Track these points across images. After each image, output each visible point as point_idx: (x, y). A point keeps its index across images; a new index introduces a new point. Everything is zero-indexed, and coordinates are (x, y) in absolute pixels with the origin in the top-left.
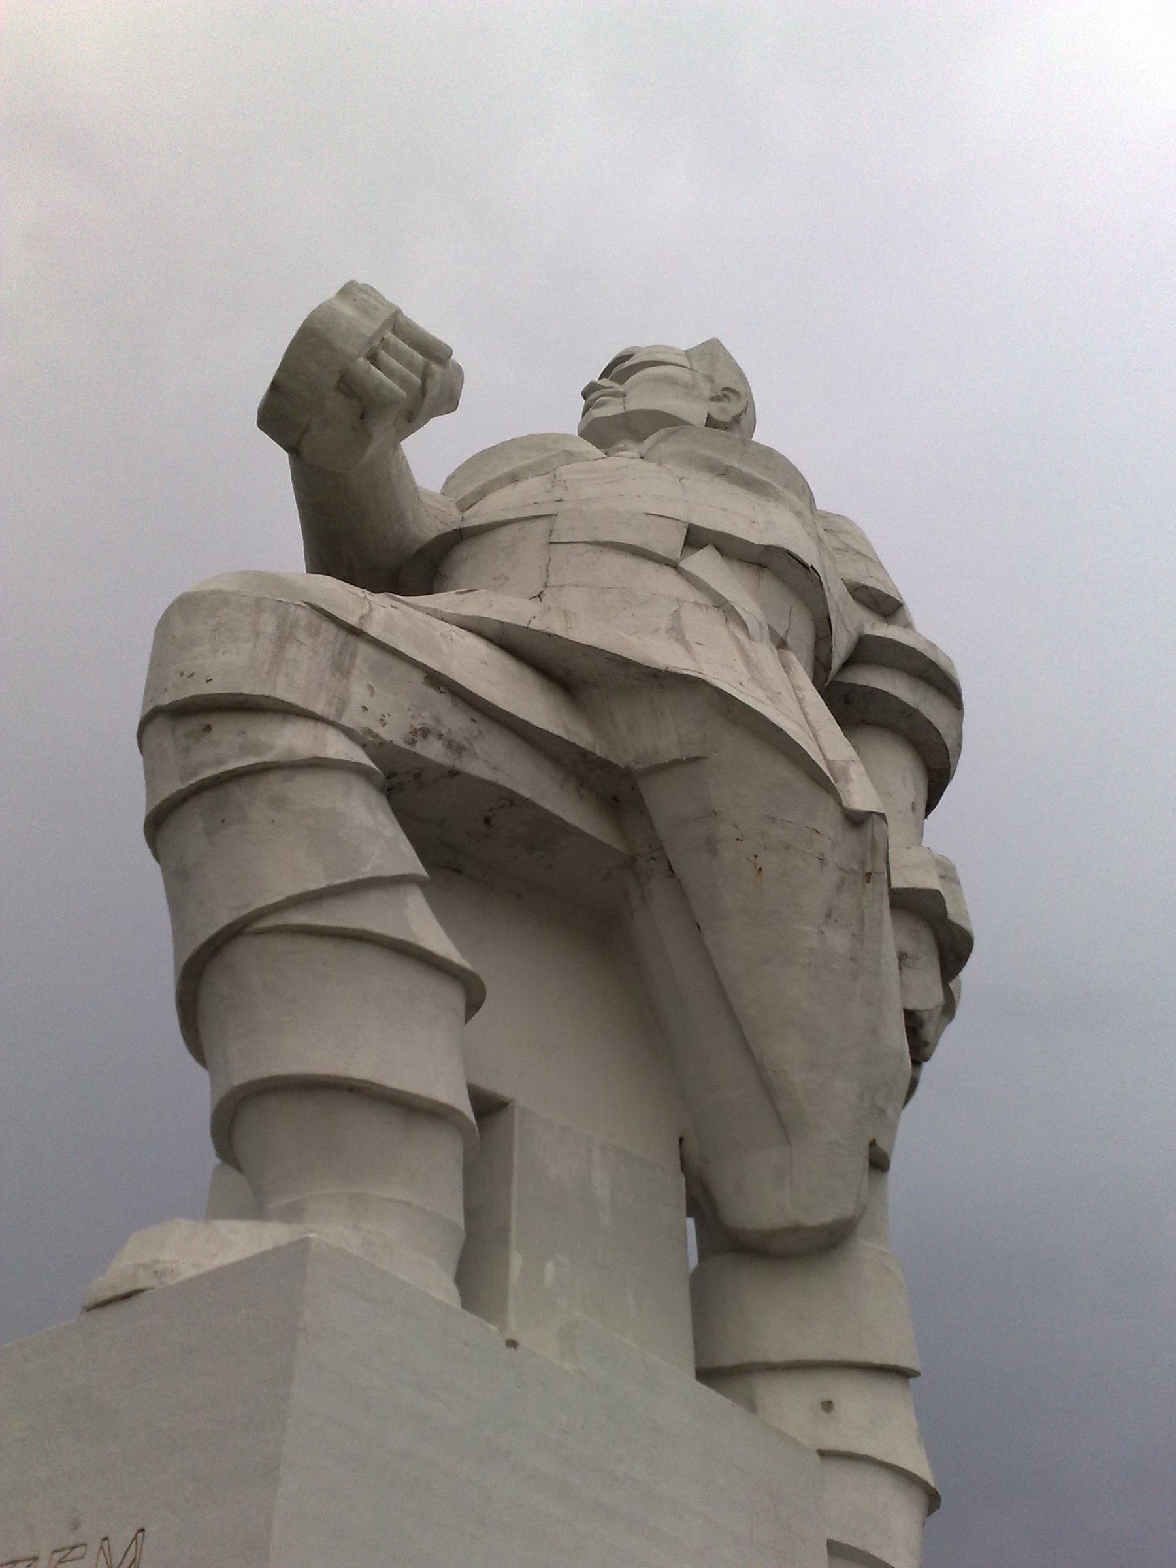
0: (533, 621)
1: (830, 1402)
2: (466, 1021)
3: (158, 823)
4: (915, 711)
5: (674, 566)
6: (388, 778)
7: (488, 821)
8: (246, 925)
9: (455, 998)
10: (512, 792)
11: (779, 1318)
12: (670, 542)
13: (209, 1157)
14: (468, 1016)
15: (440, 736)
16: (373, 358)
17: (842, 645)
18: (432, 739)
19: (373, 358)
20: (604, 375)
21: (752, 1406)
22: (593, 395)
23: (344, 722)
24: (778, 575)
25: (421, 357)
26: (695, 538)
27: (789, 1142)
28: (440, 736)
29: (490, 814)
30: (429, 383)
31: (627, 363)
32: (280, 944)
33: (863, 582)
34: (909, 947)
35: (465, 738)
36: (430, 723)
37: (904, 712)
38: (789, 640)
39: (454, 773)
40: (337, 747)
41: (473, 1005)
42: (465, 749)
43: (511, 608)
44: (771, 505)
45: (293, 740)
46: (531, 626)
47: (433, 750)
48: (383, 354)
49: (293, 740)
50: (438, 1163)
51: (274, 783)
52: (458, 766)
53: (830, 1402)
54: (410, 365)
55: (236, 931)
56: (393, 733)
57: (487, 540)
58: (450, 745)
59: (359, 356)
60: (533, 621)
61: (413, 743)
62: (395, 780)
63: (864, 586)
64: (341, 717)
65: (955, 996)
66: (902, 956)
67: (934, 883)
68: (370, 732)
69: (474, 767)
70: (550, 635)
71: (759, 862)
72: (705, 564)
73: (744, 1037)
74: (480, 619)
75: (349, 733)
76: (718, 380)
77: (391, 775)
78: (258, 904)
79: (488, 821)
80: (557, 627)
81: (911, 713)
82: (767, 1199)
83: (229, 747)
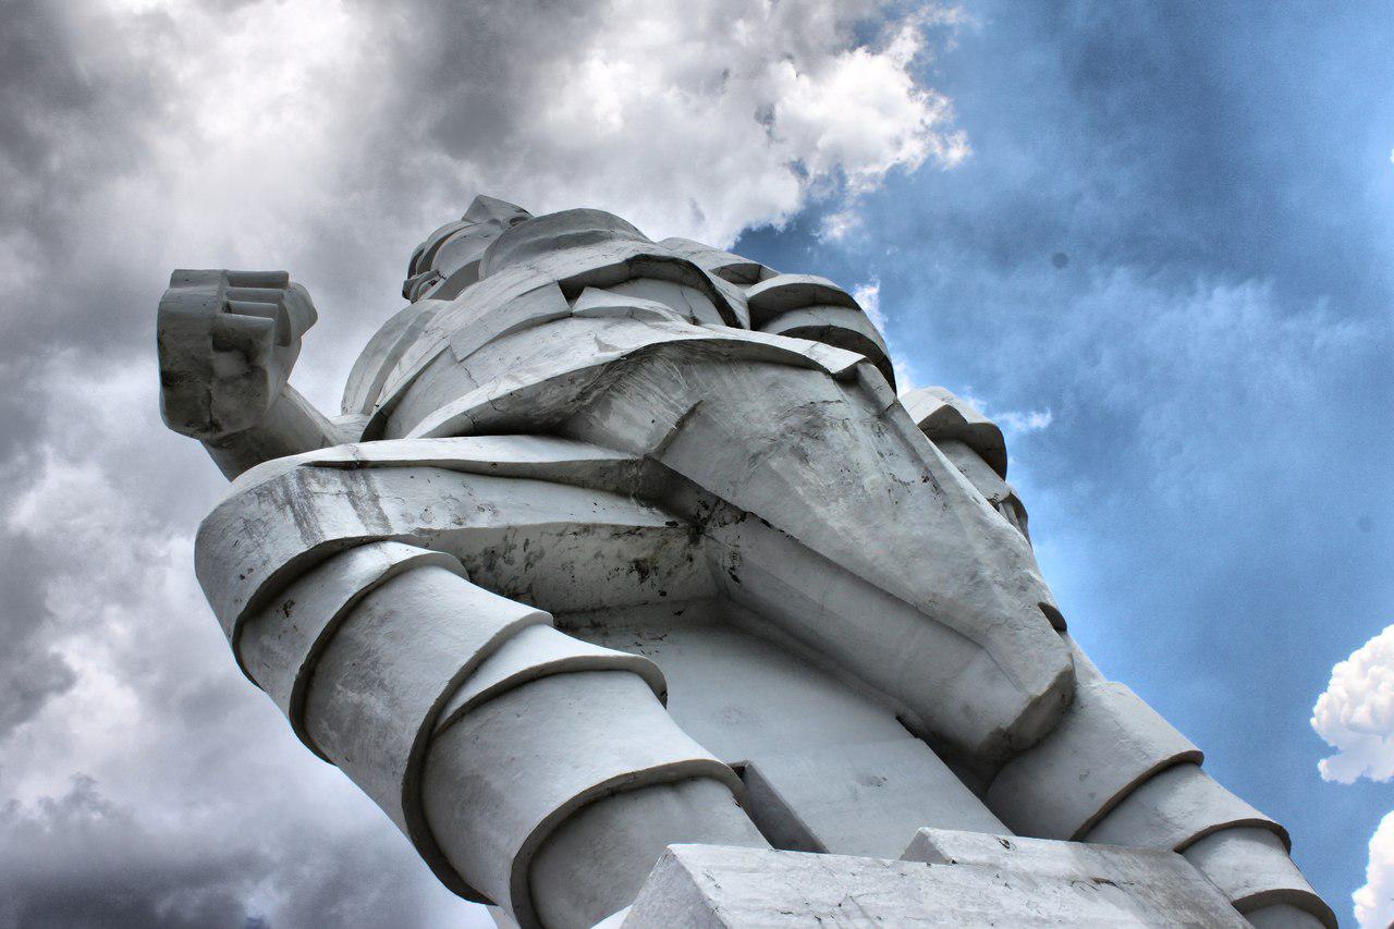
3: (302, 718)
5: (571, 315)
8: (434, 724)
9: (639, 691)
11: (1078, 776)
12: (558, 303)
13: (1051, 602)
14: (664, 701)
16: (228, 309)
19: (228, 309)
20: (412, 271)
22: (413, 291)
24: (654, 277)
26: (572, 289)
27: (982, 647)
31: (424, 254)
32: (468, 728)
44: (610, 244)
45: (368, 564)
49: (368, 564)
50: (720, 804)
51: (379, 604)
55: (434, 731)
57: (407, 402)
65: (878, 343)
67: (944, 403)
68: (422, 531)
72: (591, 300)
73: (889, 595)
76: (501, 218)
78: (429, 702)
82: (994, 699)
83: (319, 606)
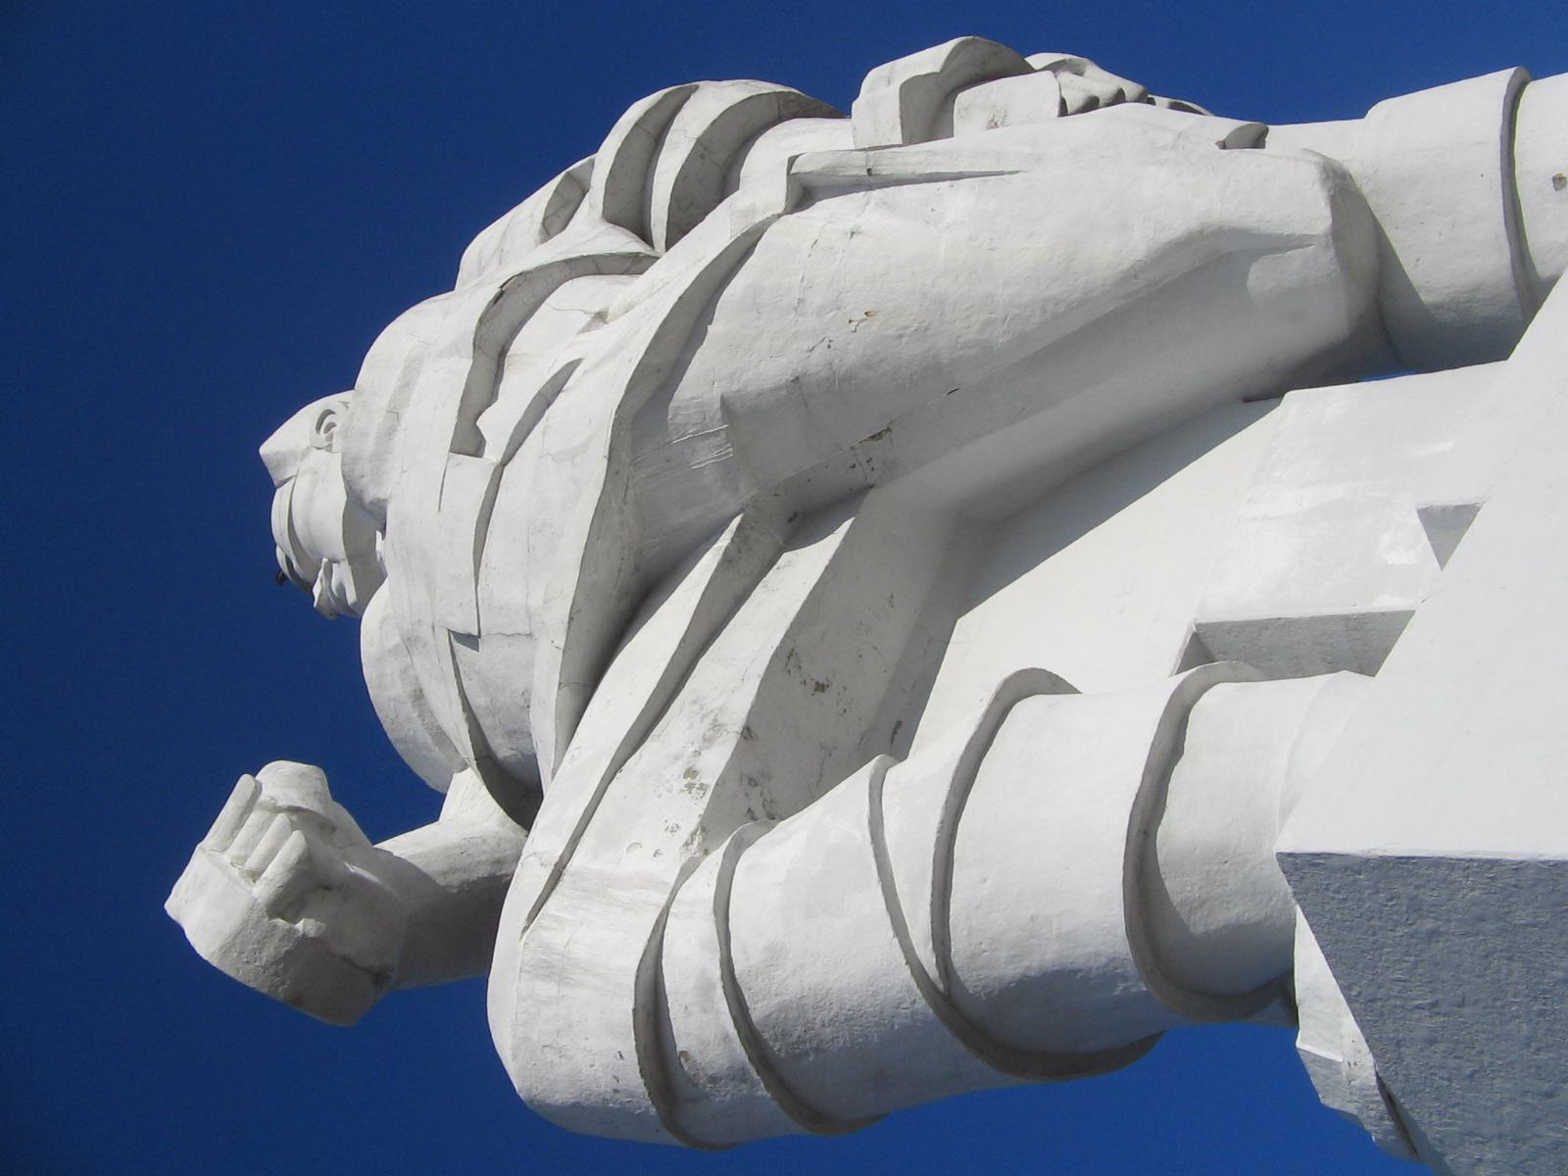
0: (556, 643)
1: (1555, 179)
2: (1076, 691)
4: (699, 141)
6: (754, 819)
7: (821, 687)
10: (776, 655)
12: (473, 473)
15: (698, 753)
16: (255, 875)
17: (624, 242)
18: (700, 764)
19: (255, 875)
21: (1552, 282)
23: (672, 880)
25: (252, 816)
26: (468, 442)
28: (698, 753)
29: (811, 685)
30: (282, 803)
33: (539, 226)
34: (982, 118)
35: (702, 720)
36: (679, 768)
37: (702, 157)
38: (596, 309)
39: (747, 733)
40: (702, 886)
41: (1051, 684)
42: (715, 720)
43: (545, 675)
46: (562, 645)
47: (715, 762)
48: (252, 863)
52: (738, 727)
53: (1555, 179)
54: (263, 827)
56: (691, 811)
58: (708, 741)
59: (250, 892)
60: (556, 643)
61: (702, 787)
62: (759, 811)
63: (543, 223)
64: (665, 883)
66: (993, 125)
69: (739, 706)
70: (571, 619)
71: (859, 315)
74: (558, 716)
75: (687, 872)
77: (751, 815)
79: (821, 687)
80: (562, 609)
81: (702, 147)
